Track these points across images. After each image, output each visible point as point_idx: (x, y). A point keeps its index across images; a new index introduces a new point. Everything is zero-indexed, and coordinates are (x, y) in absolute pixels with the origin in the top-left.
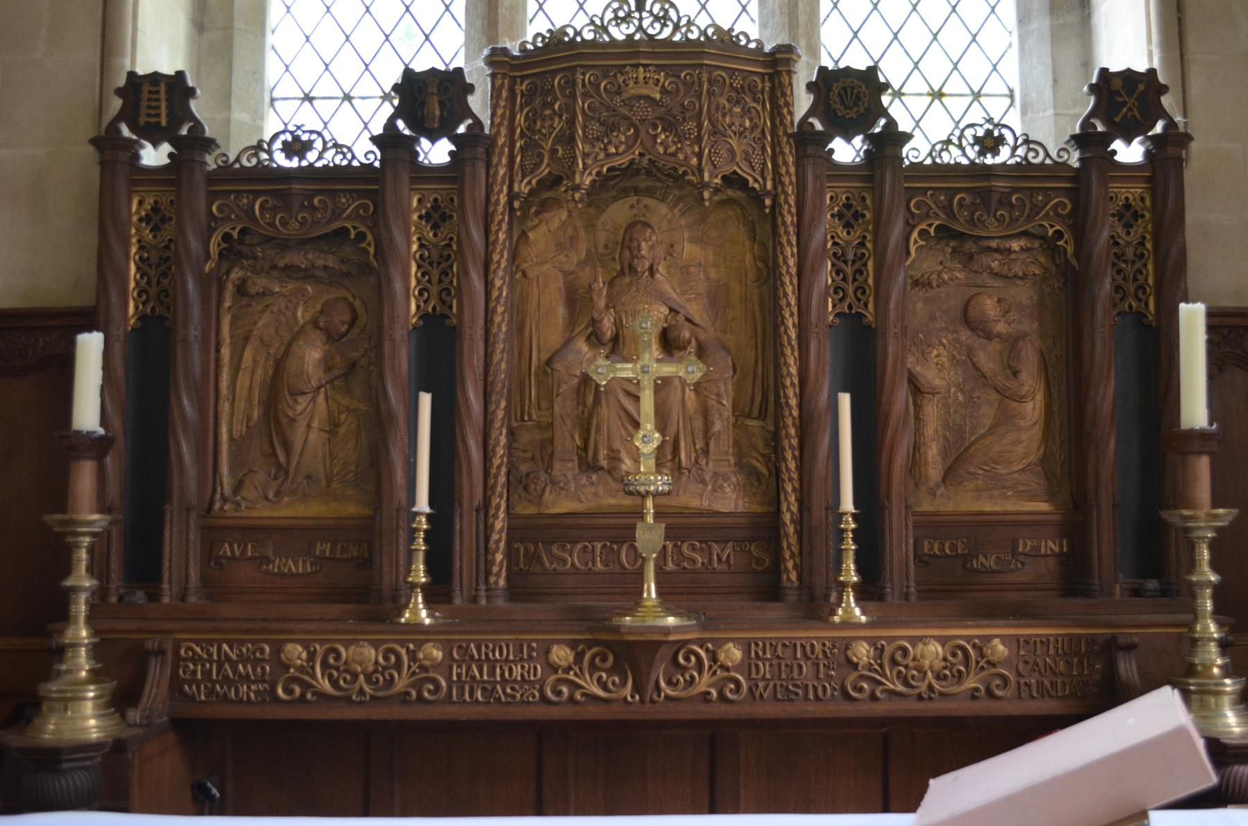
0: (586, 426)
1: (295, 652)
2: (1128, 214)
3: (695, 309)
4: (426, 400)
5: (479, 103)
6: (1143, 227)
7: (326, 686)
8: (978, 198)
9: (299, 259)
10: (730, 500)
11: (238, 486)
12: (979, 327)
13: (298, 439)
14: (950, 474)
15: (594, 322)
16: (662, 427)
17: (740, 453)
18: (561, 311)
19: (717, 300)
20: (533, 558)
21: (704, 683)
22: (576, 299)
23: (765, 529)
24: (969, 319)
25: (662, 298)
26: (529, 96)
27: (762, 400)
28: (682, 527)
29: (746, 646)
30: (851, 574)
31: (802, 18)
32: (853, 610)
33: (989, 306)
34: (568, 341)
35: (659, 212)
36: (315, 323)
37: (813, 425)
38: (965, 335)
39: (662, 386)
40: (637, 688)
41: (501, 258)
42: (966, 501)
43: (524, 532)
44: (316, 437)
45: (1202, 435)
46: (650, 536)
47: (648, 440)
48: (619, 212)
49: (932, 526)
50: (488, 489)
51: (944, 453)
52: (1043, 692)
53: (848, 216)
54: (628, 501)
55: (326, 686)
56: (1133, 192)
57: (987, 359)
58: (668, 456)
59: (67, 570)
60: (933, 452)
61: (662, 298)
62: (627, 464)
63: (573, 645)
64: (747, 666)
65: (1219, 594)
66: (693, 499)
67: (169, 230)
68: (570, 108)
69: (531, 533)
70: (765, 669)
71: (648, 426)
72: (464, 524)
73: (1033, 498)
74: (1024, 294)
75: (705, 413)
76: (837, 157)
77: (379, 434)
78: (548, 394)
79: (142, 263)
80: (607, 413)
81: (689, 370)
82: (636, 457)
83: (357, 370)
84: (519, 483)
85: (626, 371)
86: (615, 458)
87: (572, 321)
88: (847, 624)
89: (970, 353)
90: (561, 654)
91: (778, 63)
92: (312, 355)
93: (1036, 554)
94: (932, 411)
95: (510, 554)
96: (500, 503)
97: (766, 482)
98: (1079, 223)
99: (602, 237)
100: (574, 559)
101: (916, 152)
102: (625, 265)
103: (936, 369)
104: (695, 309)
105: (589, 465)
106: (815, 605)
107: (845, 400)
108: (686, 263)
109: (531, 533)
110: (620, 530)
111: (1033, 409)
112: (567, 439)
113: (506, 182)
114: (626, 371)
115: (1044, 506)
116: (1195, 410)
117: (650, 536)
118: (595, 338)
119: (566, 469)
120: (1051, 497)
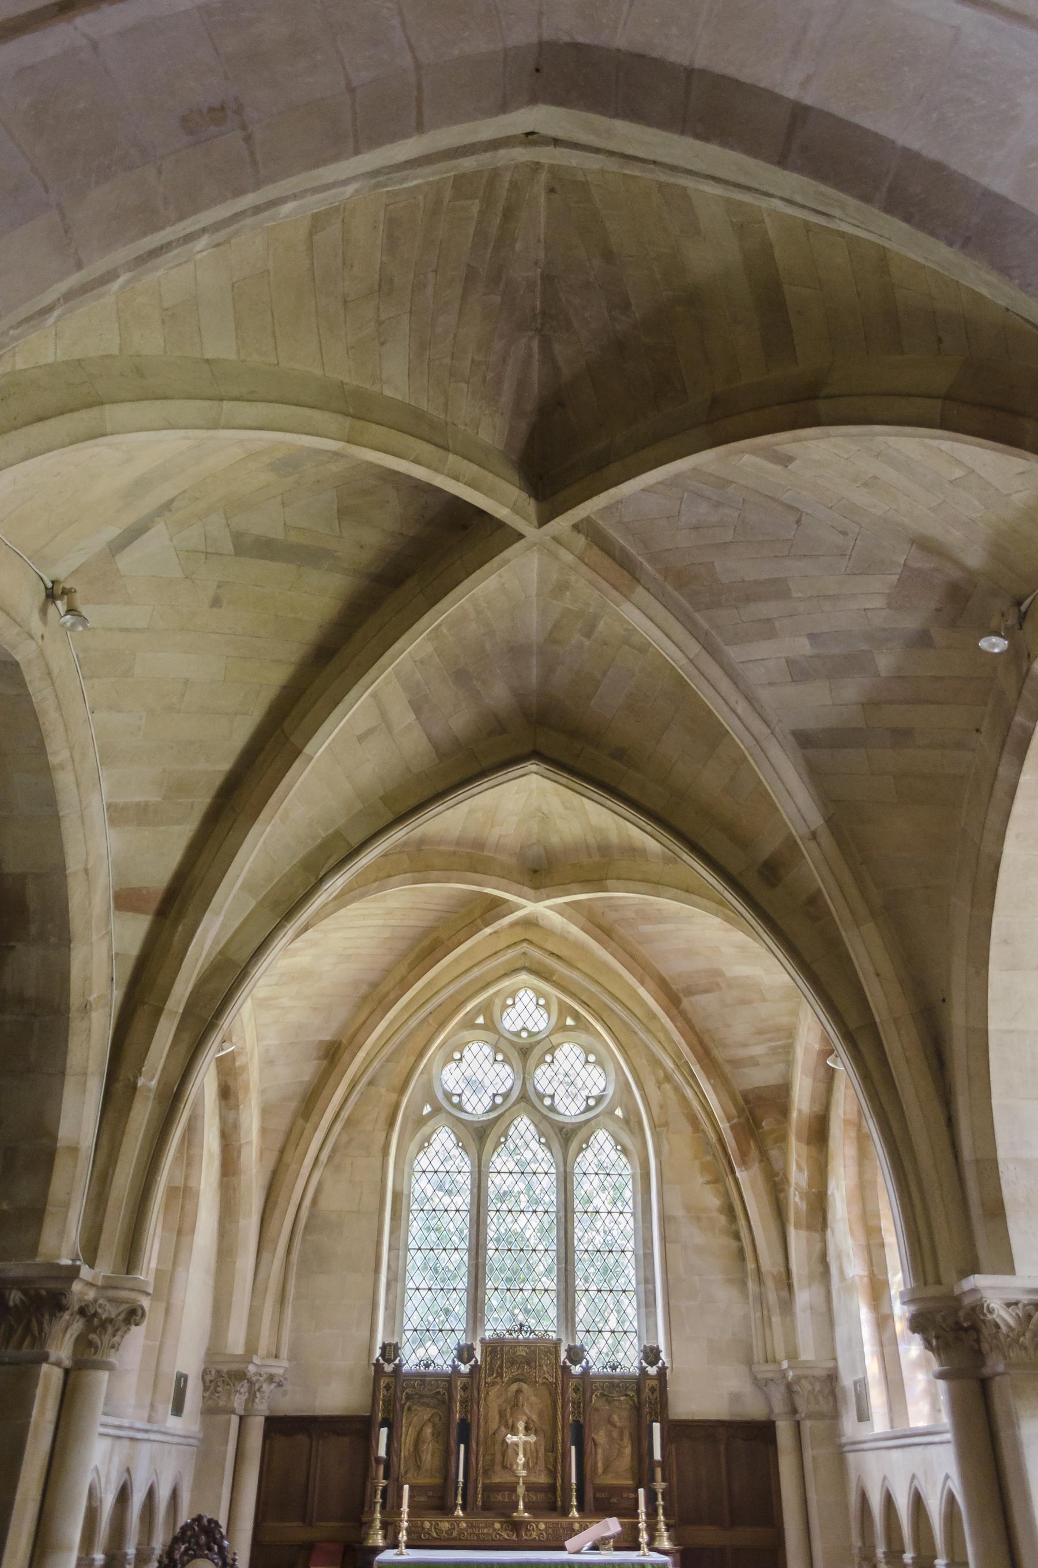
0: (504, 1455)
1: (427, 1525)
2: (653, 1390)
3: (534, 1417)
4: (462, 1446)
5: (478, 1354)
6: (657, 1394)
7: (434, 1534)
8: (614, 1385)
9: (425, 1400)
10: (543, 1479)
11: (406, 1472)
12: (614, 1425)
13: (424, 1458)
14: (606, 1470)
15: (507, 1422)
16: (525, 1456)
17: (546, 1464)
18: (497, 1417)
19: (540, 1415)
20: (489, 1497)
21: (534, 1535)
22: (502, 1414)
23: (552, 1488)
24: (610, 1422)
25: (525, 1414)
26: (491, 1352)
27: (552, 1448)
28: (530, 1488)
29: (546, 1523)
30: (574, 1502)
31: (569, 1308)
32: (575, 1513)
33: (615, 1418)
34: (499, 1427)
35: (525, 1386)
36: (429, 1420)
37: (566, 1455)
38: (609, 1426)
39: (525, 1443)
40: (517, 1536)
41: (482, 1402)
42: (610, 1480)
43: (486, 1488)
44: (429, 1457)
45: (658, 1462)
46: (521, 1490)
47: (521, 1459)
48: (514, 1387)
49: (598, 1489)
50: (477, 1474)
51: (604, 1464)
52: (626, 1541)
53: (576, 1390)
54: (514, 1479)
55: (434, 1534)
56: (654, 1383)
57: (615, 1434)
58: (526, 1465)
59: (375, 1497)
60: (600, 1465)
61: (525, 1414)
62: (515, 1467)
63: (500, 1522)
64: (546, 1530)
65: (664, 1509)
66: (533, 1479)
67: (391, 1391)
68: (502, 1357)
69: (488, 1489)
70: (550, 1531)
71: (521, 1456)
72: (471, 1485)
73: (627, 1479)
74: (625, 1414)
75: (537, 1451)
76: (573, 1372)
77: (447, 1457)
78: (494, 1443)
79: (384, 1400)
80: (510, 1451)
81: (532, 1439)
82: (517, 1465)
83: (442, 1434)
84: (486, 1472)
85: (515, 1439)
86: (512, 1465)
87: (500, 1421)
88: (573, 1518)
89: (610, 1432)
90: (497, 1526)
91: (557, 1343)
92: (428, 1431)
93: (628, 1498)
94: (600, 1451)
95: (483, 1495)
96: (480, 1479)
97: (552, 1473)
98: (638, 1391)
99: (509, 1394)
100: (500, 1498)
101: (594, 1370)
102: (515, 1404)
103: (601, 1437)
104: (534, 1417)
105: (504, 1467)
106: (565, 1512)
107: (573, 1448)
108: (533, 1402)
109: (488, 1489)
110: (512, 1489)
111: (628, 1451)
112: (498, 1458)
113: (485, 1378)
114: (515, 1439)
115: (630, 1482)
116: (657, 1456)
117: (521, 1490)
118: (506, 1425)
119: (498, 1468)
120: (633, 1479)
